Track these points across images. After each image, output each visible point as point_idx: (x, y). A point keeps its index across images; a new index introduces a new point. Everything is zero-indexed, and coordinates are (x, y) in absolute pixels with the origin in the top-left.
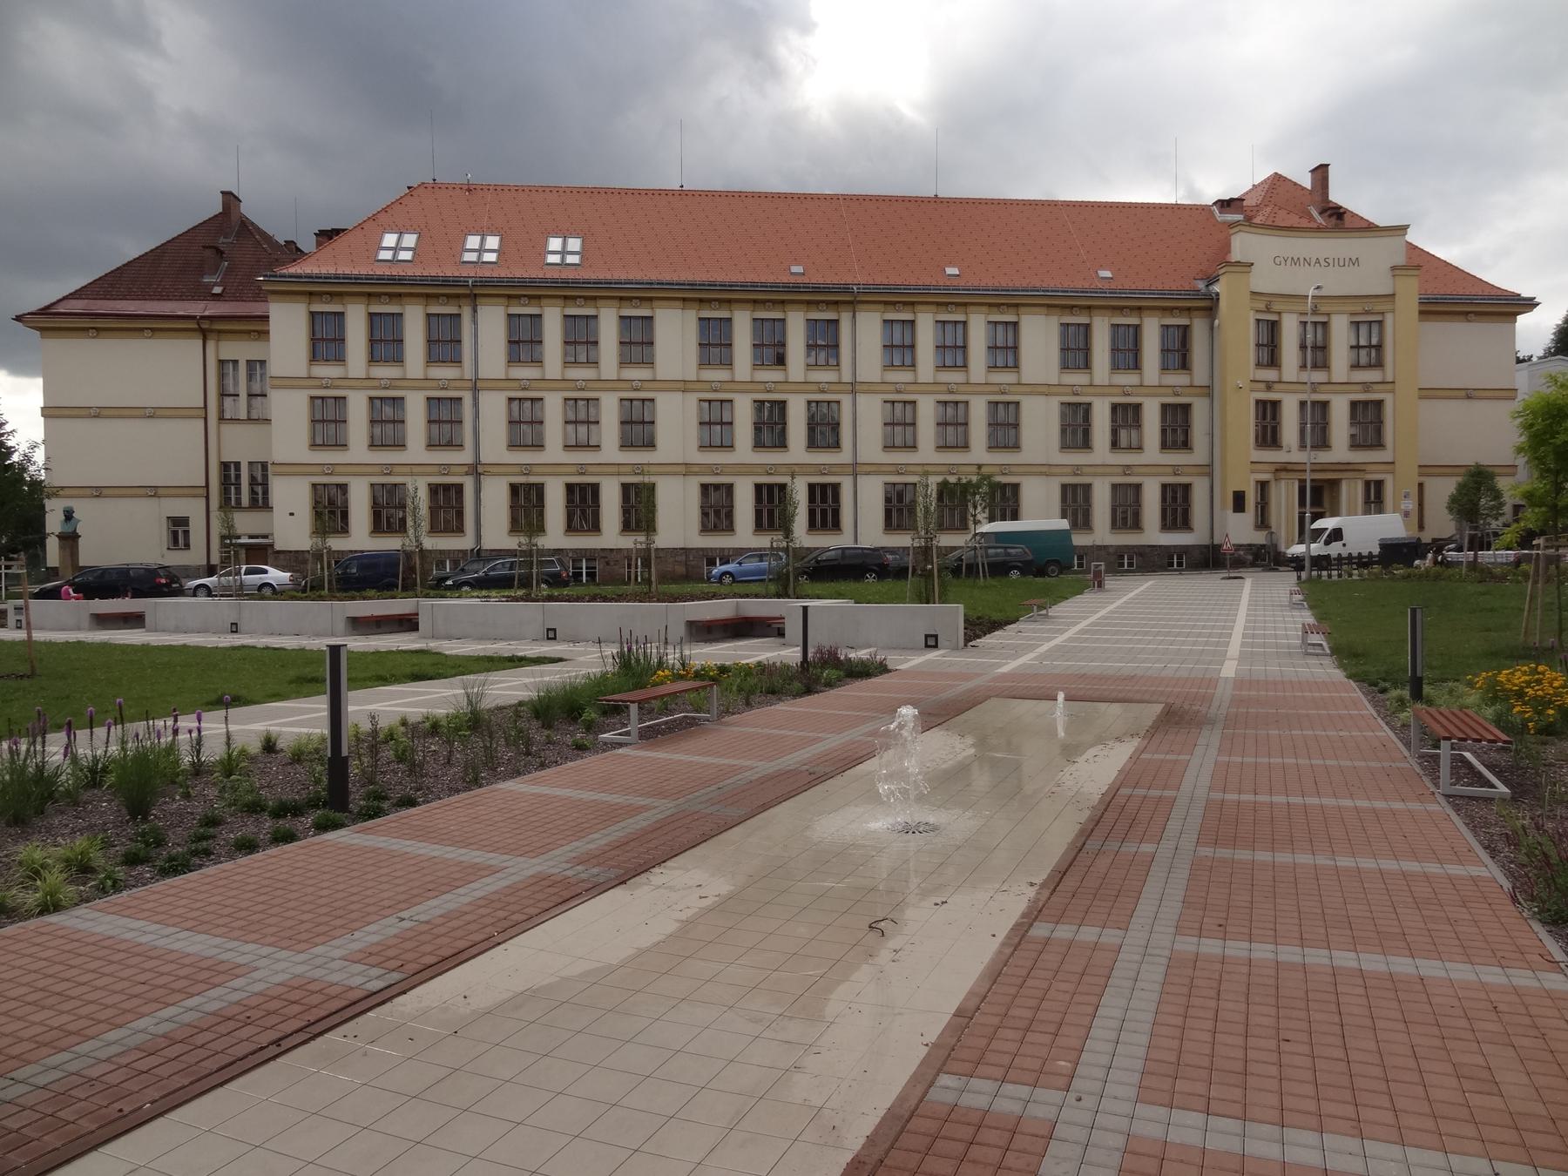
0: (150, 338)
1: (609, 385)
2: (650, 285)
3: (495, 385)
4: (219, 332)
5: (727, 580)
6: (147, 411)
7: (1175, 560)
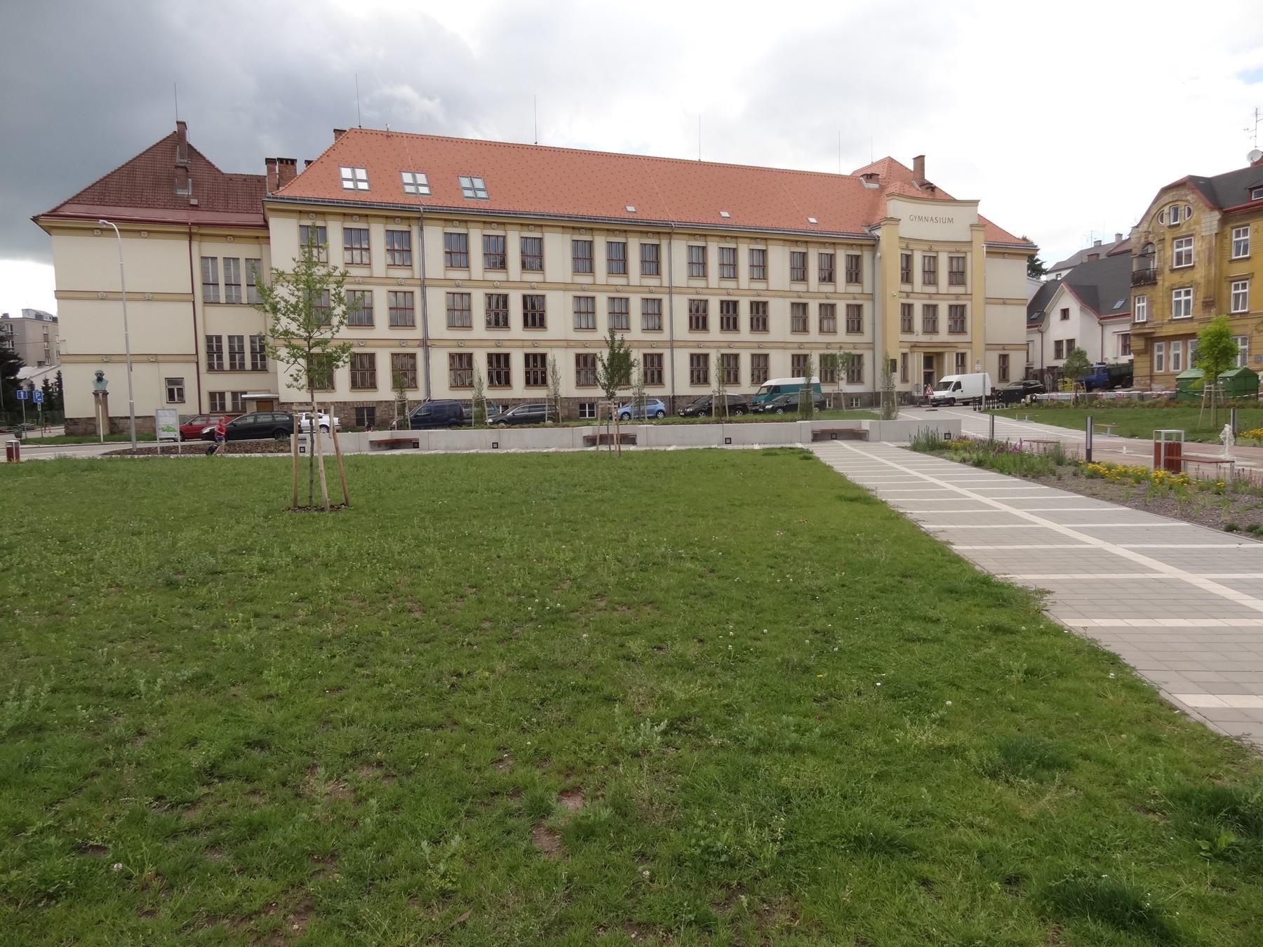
0: (146, 238)
1: (380, 281)
2: (543, 217)
3: (438, 283)
4: (202, 235)
5: (626, 417)
6: (99, 294)
7: (587, 410)
